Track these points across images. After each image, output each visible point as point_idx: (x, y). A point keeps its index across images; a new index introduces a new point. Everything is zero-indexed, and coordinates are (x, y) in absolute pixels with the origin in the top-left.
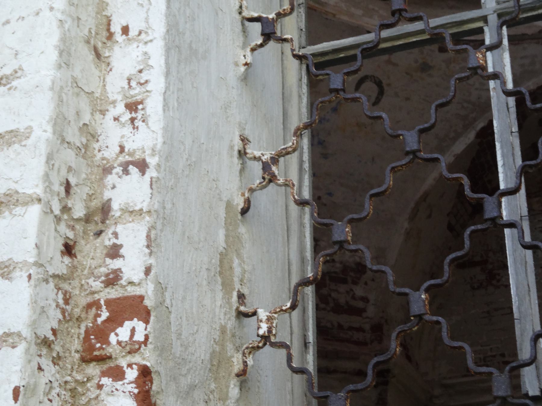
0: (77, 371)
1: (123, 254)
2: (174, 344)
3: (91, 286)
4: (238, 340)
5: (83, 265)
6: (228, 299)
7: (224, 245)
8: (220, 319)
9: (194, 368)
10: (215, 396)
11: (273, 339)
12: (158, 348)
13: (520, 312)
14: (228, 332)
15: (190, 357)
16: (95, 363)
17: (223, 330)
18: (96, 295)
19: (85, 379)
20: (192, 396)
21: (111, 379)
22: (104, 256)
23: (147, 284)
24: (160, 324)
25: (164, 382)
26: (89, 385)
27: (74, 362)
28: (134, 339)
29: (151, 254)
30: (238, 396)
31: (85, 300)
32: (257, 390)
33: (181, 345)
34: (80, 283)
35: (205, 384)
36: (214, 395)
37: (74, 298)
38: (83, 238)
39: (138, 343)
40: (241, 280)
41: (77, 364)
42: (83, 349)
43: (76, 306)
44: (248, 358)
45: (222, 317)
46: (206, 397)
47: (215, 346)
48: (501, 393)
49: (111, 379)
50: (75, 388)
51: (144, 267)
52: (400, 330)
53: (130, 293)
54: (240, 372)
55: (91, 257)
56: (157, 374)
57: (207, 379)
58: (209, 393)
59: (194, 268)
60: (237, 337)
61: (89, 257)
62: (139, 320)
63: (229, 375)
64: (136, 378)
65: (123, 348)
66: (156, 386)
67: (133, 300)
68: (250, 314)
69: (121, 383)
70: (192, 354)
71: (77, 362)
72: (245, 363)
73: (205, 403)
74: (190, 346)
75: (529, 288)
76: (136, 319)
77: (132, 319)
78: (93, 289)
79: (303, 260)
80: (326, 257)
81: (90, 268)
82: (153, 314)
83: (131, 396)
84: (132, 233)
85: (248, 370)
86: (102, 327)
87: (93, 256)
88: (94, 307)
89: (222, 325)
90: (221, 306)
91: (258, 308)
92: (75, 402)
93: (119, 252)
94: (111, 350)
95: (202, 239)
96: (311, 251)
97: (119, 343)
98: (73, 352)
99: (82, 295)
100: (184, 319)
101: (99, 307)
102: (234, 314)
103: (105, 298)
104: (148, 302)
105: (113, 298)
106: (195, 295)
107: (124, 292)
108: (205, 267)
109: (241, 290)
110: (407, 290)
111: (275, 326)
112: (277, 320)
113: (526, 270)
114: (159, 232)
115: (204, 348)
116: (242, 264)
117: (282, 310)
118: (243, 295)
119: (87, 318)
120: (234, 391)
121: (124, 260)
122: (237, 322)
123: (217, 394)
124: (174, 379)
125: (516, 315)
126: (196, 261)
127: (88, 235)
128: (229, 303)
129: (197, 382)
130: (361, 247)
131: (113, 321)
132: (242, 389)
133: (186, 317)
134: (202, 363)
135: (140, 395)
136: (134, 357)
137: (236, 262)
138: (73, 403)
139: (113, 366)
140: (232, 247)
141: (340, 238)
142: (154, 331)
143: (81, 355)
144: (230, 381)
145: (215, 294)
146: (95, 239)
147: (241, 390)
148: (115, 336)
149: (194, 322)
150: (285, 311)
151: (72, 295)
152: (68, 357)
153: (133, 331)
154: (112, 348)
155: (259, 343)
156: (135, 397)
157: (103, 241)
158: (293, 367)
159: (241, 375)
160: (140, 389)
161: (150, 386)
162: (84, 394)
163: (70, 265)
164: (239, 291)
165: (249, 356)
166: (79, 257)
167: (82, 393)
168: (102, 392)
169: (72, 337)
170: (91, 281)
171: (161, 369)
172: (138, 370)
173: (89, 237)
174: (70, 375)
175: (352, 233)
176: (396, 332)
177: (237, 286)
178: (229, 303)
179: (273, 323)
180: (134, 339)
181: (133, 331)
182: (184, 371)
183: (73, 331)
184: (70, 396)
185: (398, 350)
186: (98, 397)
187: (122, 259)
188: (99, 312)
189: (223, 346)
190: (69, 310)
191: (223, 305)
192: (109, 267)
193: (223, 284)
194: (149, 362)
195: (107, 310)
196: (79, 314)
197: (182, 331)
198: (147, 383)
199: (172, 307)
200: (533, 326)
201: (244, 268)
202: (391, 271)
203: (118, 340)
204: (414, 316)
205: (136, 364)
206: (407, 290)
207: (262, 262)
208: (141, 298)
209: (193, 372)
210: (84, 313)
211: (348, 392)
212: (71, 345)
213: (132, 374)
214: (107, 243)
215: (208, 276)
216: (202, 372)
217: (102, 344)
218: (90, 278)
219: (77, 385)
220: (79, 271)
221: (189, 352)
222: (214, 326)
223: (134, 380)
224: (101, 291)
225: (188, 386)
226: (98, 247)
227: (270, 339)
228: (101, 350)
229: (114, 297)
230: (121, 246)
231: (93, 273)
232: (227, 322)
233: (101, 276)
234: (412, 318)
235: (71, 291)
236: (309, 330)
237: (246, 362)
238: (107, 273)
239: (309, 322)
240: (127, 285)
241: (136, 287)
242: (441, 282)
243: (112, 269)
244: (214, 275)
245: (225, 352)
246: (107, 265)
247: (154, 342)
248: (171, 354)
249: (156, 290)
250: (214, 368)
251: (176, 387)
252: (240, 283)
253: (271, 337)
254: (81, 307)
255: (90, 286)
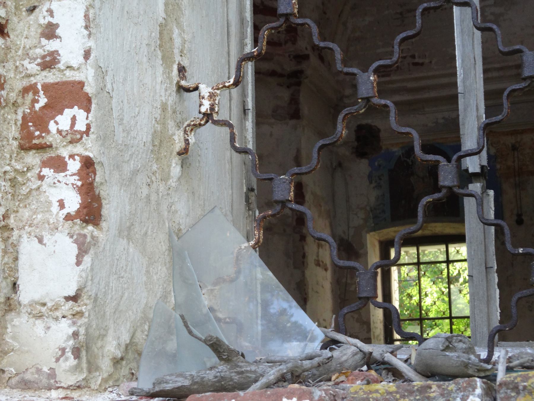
0: (15, 160)
1: (60, 35)
2: (116, 131)
3: (27, 69)
4: (179, 115)
5: (17, 45)
6: (169, 74)
7: (164, 15)
8: (161, 96)
9: (137, 153)
10: (157, 177)
11: (215, 117)
12: (101, 138)
13: (464, 86)
14: (169, 110)
15: (132, 142)
16: (34, 151)
17: (164, 108)
18: (32, 78)
19: (25, 169)
20: (135, 182)
21: (52, 170)
22: (38, 36)
23: (87, 70)
24: (102, 112)
25: (107, 172)
26: (29, 174)
27: (12, 150)
28: (75, 129)
29: (89, 35)
30: (180, 174)
31: (21, 84)
32: (197, 164)
33: (124, 131)
34: (14, 65)
35: (147, 166)
36: (156, 176)
37: (9, 82)
38: (15, 14)
39: (79, 133)
40: (181, 52)
41: (15, 152)
42: (21, 137)
43: (12, 90)
44: (189, 136)
45: (163, 94)
46: (149, 180)
47: (156, 125)
48: (447, 183)
49: (52, 170)
50: (15, 178)
51: (83, 50)
52: (347, 112)
53: (69, 78)
54: (181, 150)
55: (25, 36)
56: (100, 165)
57: (149, 161)
58: (151, 174)
59: (134, 46)
60: (178, 113)
61: (23, 36)
62: (79, 108)
63: (171, 154)
64: (79, 170)
65: (64, 137)
66: (100, 177)
67: (73, 86)
68: (191, 89)
69: (63, 174)
70: (134, 138)
71: (15, 151)
72: (187, 141)
73: (147, 187)
74: (131, 130)
75: (475, 61)
76: (76, 107)
77: (72, 107)
78: (29, 72)
79: (242, 21)
80: (271, 31)
81: (24, 48)
82: (94, 101)
83: (74, 188)
84: (69, 12)
85: (190, 148)
86: (41, 114)
87: (26, 35)
88: (31, 91)
89: (162, 102)
90: (162, 82)
91: (200, 83)
92: (15, 192)
93: (55, 32)
94: (51, 139)
95: (142, 13)
96: (251, 10)
97: (59, 132)
98: (11, 139)
99: (18, 77)
100: (125, 101)
101: (36, 92)
102: (174, 88)
103: (42, 82)
104: (89, 89)
105: (51, 83)
106: (136, 74)
107: (62, 76)
108: (145, 42)
109: (181, 63)
110: (355, 70)
111: (217, 103)
112: (219, 97)
113: (473, 42)
114: (97, 11)
115: (145, 130)
116: (182, 33)
117: (225, 86)
118: (184, 67)
119: (24, 103)
120: (176, 170)
121: (61, 41)
122: (178, 96)
123: (159, 175)
124: (118, 167)
125: (460, 89)
126: (136, 37)
127: (21, 10)
128: (169, 78)
129: (140, 166)
130: (308, 21)
131: (52, 108)
132: (183, 166)
133: (127, 100)
134: (144, 145)
135: (83, 188)
136: (75, 147)
137: (176, 31)
138: (14, 194)
139: (53, 155)
140: (172, 16)
141: (287, 10)
142: (96, 120)
143: (19, 143)
144: (172, 160)
145: (156, 70)
146: (29, 15)
147: (182, 167)
148: (55, 124)
149: (135, 104)
150: (228, 87)
151: (7, 78)
152: (6, 145)
153: (74, 119)
154: (52, 137)
155: (201, 120)
156: (78, 190)
157: (37, 19)
158: (237, 147)
159: (183, 154)
160: (84, 181)
161: (93, 178)
162: (24, 184)
163: (3, 46)
164: (179, 64)
165: (191, 134)
166: (11, 36)
167: (23, 183)
168: (43, 183)
169: (8, 124)
170: (26, 63)
171: (104, 159)
172: (80, 162)
173: (22, 12)
174: (9, 165)
175: (298, 4)
176: (343, 115)
177: (178, 59)
178: (169, 78)
179: (216, 100)
180: (75, 129)
181: (74, 119)
182: (127, 158)
183: (9, 117)
184: (10, 185)
185: (344, 132)
186: (39, 188)
187: (58, 40)
188: (37, 98)
189: (164, 124)
190: (5, 96)
191: (163, 81)
192: (44, 48)
193: (163, 58)
194: (92, 152)
195: (45, 95)
196: (15, 99)
197: (124, 116)
198: (90, 174)
199: (113, 91)
200: (477, 100)
201: (184, 38)
202: (339, 49)
203: (58, 129)
204: (362, 99)
205: (78, 155)
206: (355, 70)
207: (201, 28)
208: (81, 84)
209: (135, 156)
210: (20, 97)
211: (292, 175)
212: (8, 132)
213: (74, 166)
214: (42, 21)
215: (148, 52)
216: (144, 156)
217: (41, 133)
218: (24, 60)
219: (17, 174)
220: (13, 51)
221: (131, 136)
222: (155, 105)
223: (77, 172)
224: (37, 74)
225: (132, 172)
226: (32, 24)
227: (213, 116)
228: (41, 139)
229: (52, 81)
230: (57, 26)
231: (28, 54)
232: (168, 98)
233: (37, 58)
234: (360, 101)
235: (5, 74)
236: (248, 95)
237: (188, 140)
238: (43, 55)
239: (248, 88)
240: (66, 70)
241: (76, 72)
242: (390, 63)
243: (48, 51)
244: (155, 50)
245: (167, 130)
246: (43, 46)
247: (96, 132)
248: (114, 141)
249: (96, 75)
250: (156, 148)
251: (119, 175)
252: (180, 54)
253: (214, 114)
254: (17, 91)
255: (25, 68)
